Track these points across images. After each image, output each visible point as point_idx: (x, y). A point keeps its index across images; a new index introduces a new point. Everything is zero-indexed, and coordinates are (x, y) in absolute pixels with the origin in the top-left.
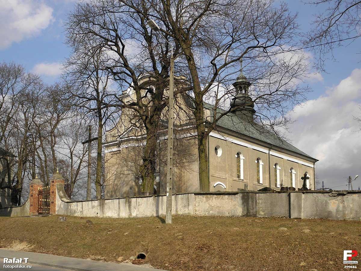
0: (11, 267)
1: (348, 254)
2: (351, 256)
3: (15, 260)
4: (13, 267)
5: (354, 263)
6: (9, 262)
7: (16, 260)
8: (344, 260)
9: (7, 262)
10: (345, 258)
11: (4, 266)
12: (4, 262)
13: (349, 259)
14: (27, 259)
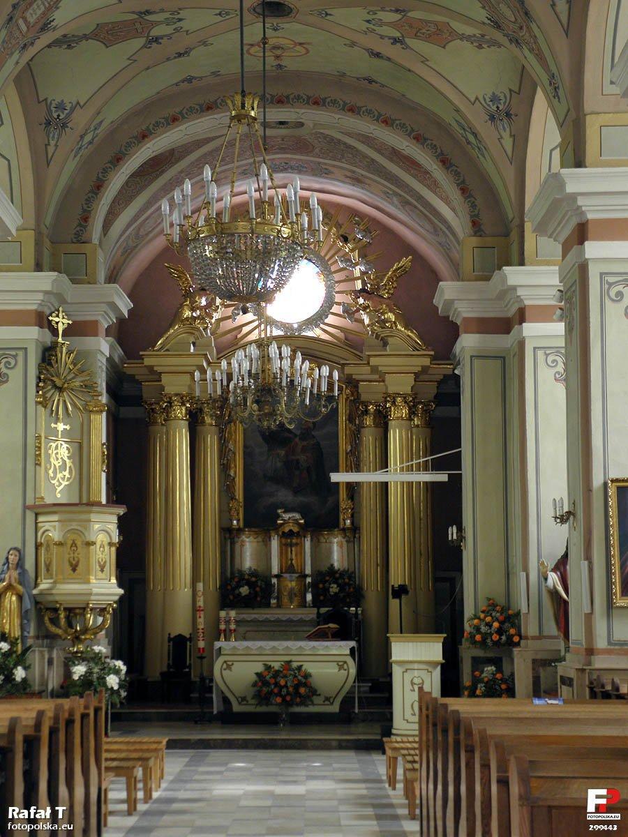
0: (24, 827)
1: (598, 797)
2: (605, 803)
3: (35, 811)
4: (31, 827)
5: (611, 819)
6: (21, 816)
7: (38, 811)
8: (588, 811)
9: (16, 817)
10: (591, 808)
11: (9, 825)
12: (10, 817)
13: (598, 808)
14: (63, 810)
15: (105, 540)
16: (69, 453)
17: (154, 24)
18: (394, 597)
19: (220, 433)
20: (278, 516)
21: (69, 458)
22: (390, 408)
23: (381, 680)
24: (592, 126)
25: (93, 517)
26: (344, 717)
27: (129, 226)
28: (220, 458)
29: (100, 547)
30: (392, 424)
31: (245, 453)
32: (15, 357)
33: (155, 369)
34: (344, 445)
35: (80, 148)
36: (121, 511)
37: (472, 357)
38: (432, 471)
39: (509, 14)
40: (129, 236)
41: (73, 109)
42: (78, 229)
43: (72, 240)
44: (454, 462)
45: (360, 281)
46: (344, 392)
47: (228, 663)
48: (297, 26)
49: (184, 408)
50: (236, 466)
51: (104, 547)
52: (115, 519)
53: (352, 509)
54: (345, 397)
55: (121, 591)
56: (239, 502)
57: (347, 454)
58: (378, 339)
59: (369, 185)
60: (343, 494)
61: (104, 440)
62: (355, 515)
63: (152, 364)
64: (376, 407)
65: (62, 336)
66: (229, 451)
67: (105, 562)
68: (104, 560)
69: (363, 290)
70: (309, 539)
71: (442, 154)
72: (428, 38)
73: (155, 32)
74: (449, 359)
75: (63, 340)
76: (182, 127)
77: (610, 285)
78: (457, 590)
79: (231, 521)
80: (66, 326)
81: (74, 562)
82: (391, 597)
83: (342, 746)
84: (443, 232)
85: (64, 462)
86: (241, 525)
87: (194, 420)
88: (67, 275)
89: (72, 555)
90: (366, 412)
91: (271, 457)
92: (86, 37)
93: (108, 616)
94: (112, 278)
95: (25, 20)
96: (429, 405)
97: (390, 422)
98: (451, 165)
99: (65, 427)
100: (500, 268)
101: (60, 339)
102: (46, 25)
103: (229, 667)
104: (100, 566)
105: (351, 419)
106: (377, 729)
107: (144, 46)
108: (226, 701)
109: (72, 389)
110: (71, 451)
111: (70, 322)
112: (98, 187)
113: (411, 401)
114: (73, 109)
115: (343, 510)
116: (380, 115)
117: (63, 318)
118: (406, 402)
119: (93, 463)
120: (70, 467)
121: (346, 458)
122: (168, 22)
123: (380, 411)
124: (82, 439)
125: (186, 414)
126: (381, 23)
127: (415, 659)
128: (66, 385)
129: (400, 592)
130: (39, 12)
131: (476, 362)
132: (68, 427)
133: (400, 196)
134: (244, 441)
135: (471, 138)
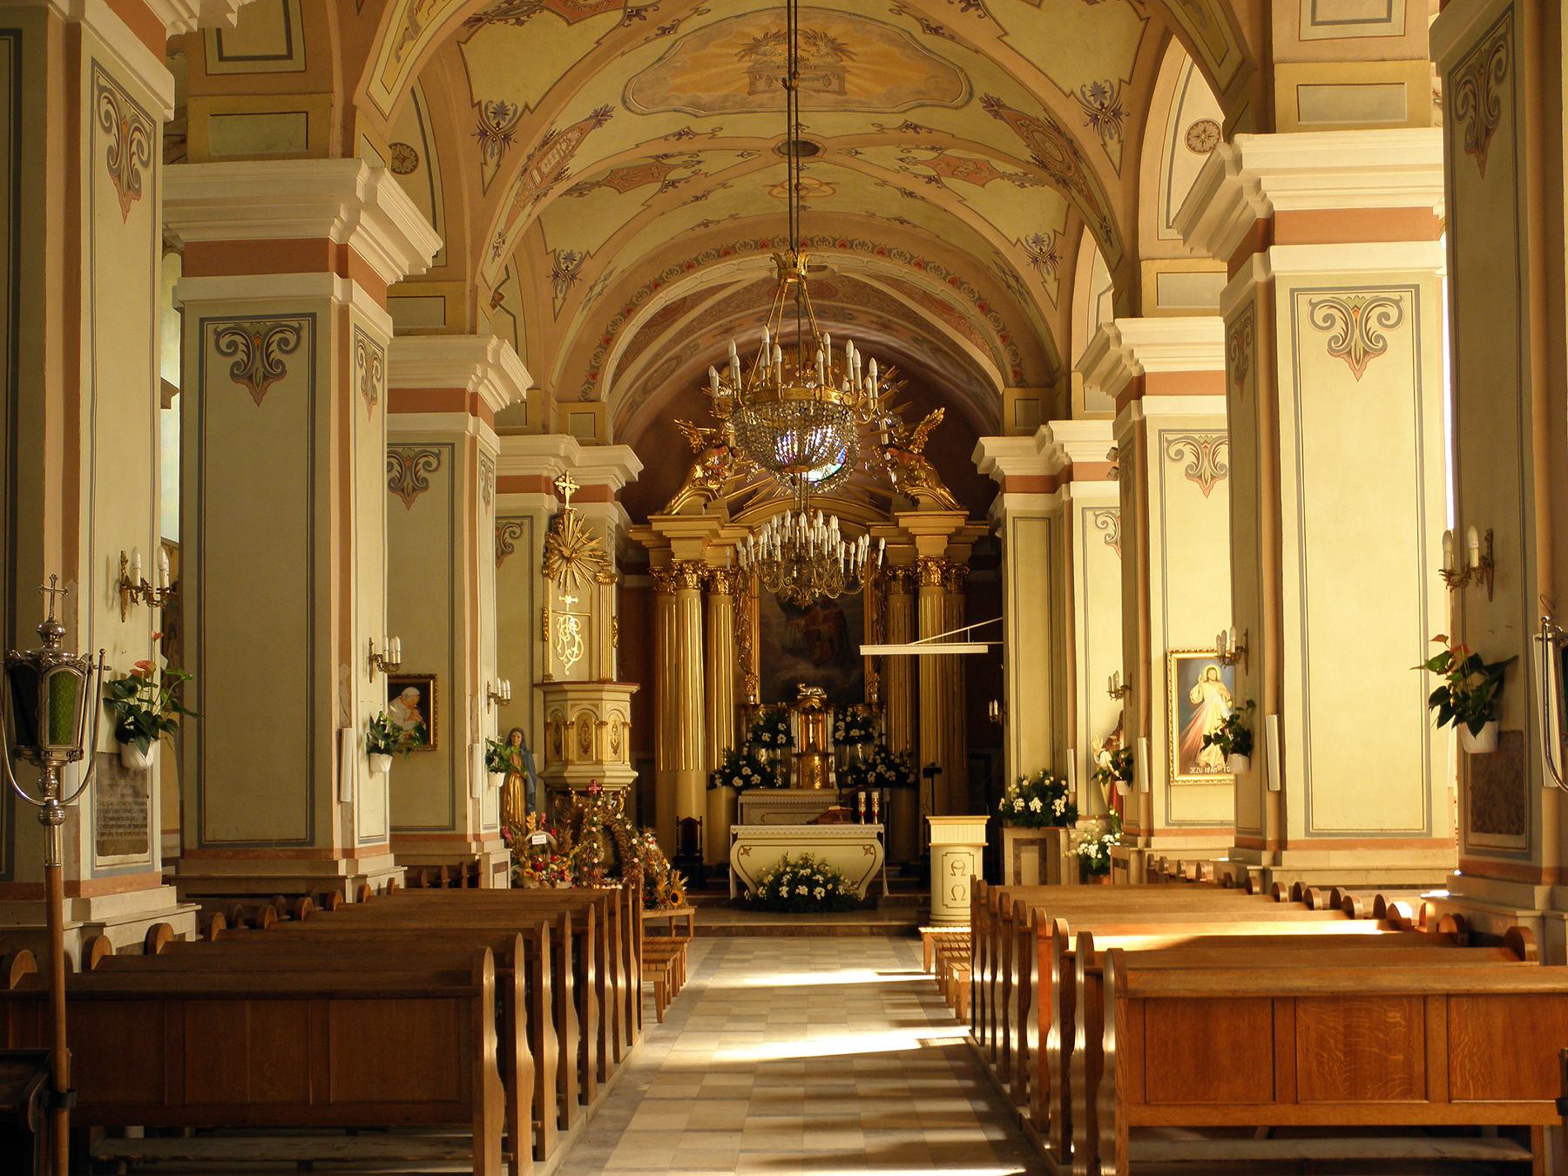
17: (673, 167)
20: (799, 691)
24: (1148, 271)
25: (605, 695)
26: (870, 904)
27: (637, 379)
28: (735, 630)
30: (923, 590)
31: (761, 624)
32: (520, 525)
34: (870, 614)
36: (635, 688)
39: (1056, 153)
41: (582, 260)
44: (995, 633)
48: (825, 166)
52: (627, 697)
60: (868, 667)
69: (890, 445)
71: (980, 298)
72: (967, 177)
73: (672, 176)
76: (698, 274)
77: (1170, 443)
83: (874, 933)
87: (707, 588)
90: (895, 577)
92: (598, 184)
94: (618, 440)
95: (539, 170)
100: (1045, 423)
102: (560, 174)
103: (746, 852)
106: (913, 914)
107: (661, 191)
108: (741, 886)
112: (608, 341)
114: (582, 260)
116: (912, 257)
119: (603, 638)
122: (686, 165)
126: (916, 162)
127: (958, 840)
129: (931, 772)
130: (553, 162)
131: (1020, 524)
135: (1012, 282)
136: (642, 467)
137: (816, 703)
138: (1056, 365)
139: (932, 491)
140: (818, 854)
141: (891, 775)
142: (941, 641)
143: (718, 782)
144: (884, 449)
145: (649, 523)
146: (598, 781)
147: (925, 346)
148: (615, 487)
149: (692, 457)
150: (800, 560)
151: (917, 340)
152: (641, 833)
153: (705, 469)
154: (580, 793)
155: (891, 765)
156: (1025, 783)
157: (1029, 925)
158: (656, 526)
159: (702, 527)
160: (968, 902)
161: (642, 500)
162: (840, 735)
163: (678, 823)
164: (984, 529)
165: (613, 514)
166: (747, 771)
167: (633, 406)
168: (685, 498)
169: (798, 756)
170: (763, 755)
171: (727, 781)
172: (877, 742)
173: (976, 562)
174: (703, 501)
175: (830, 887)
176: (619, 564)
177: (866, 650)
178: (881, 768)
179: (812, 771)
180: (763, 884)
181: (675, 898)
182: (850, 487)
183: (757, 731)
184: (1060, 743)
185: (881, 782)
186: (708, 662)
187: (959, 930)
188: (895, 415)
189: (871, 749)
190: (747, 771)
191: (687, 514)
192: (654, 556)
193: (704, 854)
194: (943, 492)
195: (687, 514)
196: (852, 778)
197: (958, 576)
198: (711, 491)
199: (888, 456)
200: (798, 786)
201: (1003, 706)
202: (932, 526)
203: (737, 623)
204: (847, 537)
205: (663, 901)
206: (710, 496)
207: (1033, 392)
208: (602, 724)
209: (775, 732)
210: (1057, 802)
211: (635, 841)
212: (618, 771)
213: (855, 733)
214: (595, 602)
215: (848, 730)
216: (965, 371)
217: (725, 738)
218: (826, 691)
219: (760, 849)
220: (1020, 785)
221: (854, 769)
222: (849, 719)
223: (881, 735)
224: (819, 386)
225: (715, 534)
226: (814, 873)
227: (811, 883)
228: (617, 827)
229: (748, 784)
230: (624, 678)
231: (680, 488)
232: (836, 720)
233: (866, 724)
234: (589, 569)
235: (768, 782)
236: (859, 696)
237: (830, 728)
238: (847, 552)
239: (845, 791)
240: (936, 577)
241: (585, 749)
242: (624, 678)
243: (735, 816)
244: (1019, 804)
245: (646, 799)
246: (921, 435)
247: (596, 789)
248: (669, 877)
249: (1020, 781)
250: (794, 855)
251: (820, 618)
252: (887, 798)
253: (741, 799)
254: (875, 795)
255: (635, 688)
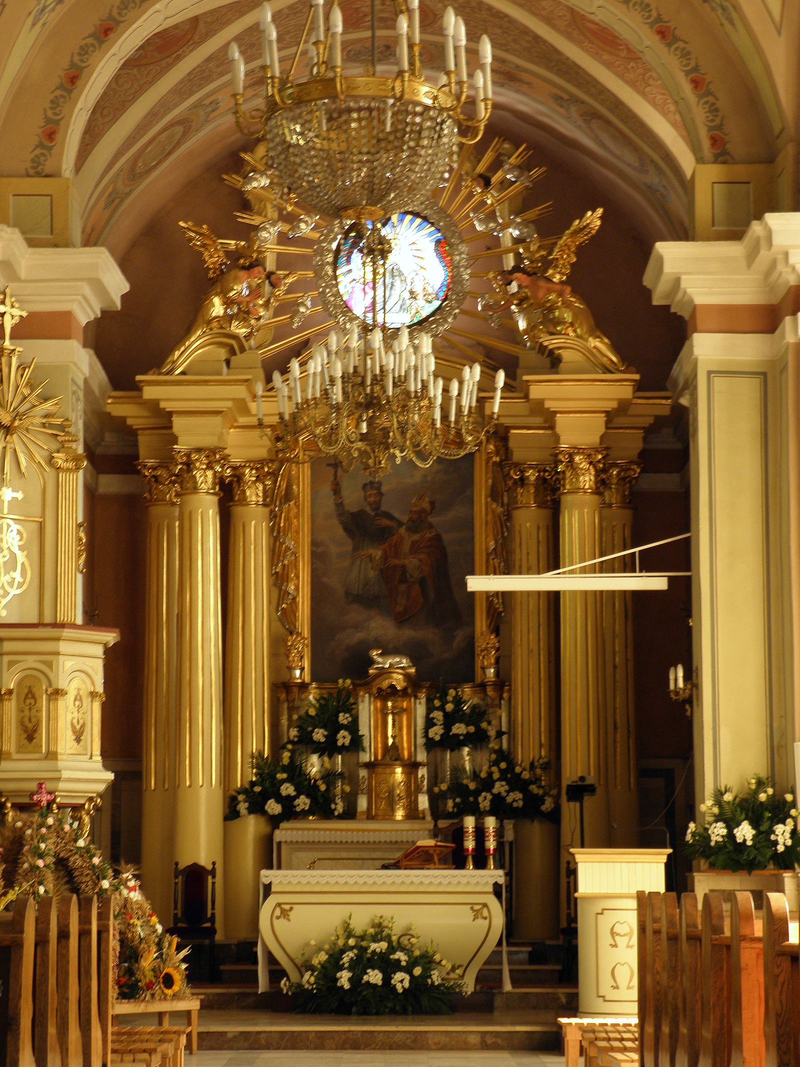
15: (83, 687)
16: (21, 540)
18: (569, 799)
19: (271, 520)
20: (372, 662)
21: (21, 548)
22: (564, 472)
23: (548, 942)
25: (63, 647)
26: (482, 1004)
28: (272, 562)
29: (75, 700)
30: (567, 500)
31: (314, 554)
33: (163, 405)
35: (43, 10)
36: (111, 637)
37: (710, 373)
38: (641, 571)
40: (117, 175)
42: (38, 151)
43: (26, 170)
44: (679, 558)
45: (511, 255)
46: (483, 448)
47: (284, 906)
49: (210, 473)
50: (298, 578)
51: (81, 700)
52: (99, 651)
53: (498, 650)
54: (484, 457)
55: (110, 776)
56: (303, 638)
57: (488, 555)
58: (543, 354)
59: (528, 84)
61: (80, 519)
62: (501, 660)
63: (158, 397)
64: (539, 471)
65: (11, 338)
66: (285, 552)
67: (83, 726)
68: (81, 722)
69: (516, 269)
70: (423, 701)
71: (659, 19)
74: (663, 388)
75: (12, 344)
78: (677, 791)
79: (290, 669)
80: (16, 320)
81: (30, 726)
82: (564, 797)
84: (656, 166)
85: (13, 556)
86: (307, 679)
87: (228, 494)
88: (23, 232)
89: (27, 712)
90: (522, 481)
91: (358, 562)
93: (87, 819)
94: (90, 240)
96: (629, 469)
97: (563, 498)
98: (676, 39)
99: (15, 495)
100: (759, 217)
101: (7, 343)
103: (285, 914)
104: (74, 732)
105: (494, 494)
108: (276, 972)
109: (27, 430)
110: (25, 536)
111: (25, 314)
112: (73, 79)
113: (599, 461)
115: (482, 651)
117: (13, 307)
118: (591, 463)
119: (62, 557)
120: (23, 564)
121: (487, 561)
123: (544, 480)
124: (43, 515)
125: (214, 484)
127: (617, 882)
128: (17, 423)
129: (578, 791)
132: (20, 495)
133: (583, 102)
134: (312, 535)
136: (125, 287)
137: (398, 680)
138: (777, 127)
139: (581, 342)
140: (401, 919)
141: (516, 798)
142: (593, 569)
143: (243, 807)
144: (507, 277)
145: (137, 388)
146: (49, 786)
147: (573, 109)
148: (84, 316)
149: (210, 282)
150: (372, 403)
151: (562, 100)
152: (117, 873)
153: (228, 303)
154: (20, 808)
155: (515, 782)
156: (728, 797)
157: (727, 933)
158: (149, 393)
159: (221, 395)
160: (634, 994)
161: (129, 345)
162: (436, 732)
163: (177, 873)
164: (661, 406)
165: (80, 362)
166: (288, 789)
167: (114, 200)
168: (195, 348)
169: (370, 766)
170: (314, 765)
171: (257, 808)
172: (493, 745)
173: (649, 459)
174: (223, 353)
175: (417, 971)
176: (90, 453)
177: (477, 583)
178: (500, 787)
179: (391, 792)
180: (312, 968)
181: (168, 981)
182: (455, 339)
183: (305, 725)
184: (783, 734)
185: (499, 808)
186: (229, 614)
187: (621, 1021)
188: (525, 223)
189: (484, 760)
190: (288, 789)
191: (197, 375)
192: (145, 442)
193: (219, 925)
194: (599, 344)
195: (197, 375)
196: (454, 801)
197: (622, 479)
198: (235, 337)
199: (514, 287)
200: (370, 816)
201: (691, 675)
202: (582, 399)
203: (276, 553)
204: (448, 370)
205: (150, 986)
206: (234, 348)
207: (741, 171)
208: (58, 693)
209: (334, 728)
210: (779, 828)
211: (105, 884)
212: (81, 770)
213: (459, 729)
214: (49, 501)
215: (447, 726)
216: (636, 149)
217: (255, 739)
218: (415, 662)
219: (309, 909)
220: (719, 802)
221: (457, 788)
222: (449, 707)
223: (500, 734)
224: (400, 73)
225: (242, 407)
226: (392, 949)
227: (388, 966)
228: (76, 861)
229: (289, 813)
230: (94, 617)
231: (188, 331)
232: (430, 709)
233: (477, 716)
234: (40, 446)
235: (322, 808)
236: (463, 668)
237: (420, 722)
238: (446, 390)
239: (443, 824)
240: (587, 480)
241: (30, 733)
242: (94, 617)
243: (269, 855)
244: (718, 831)
245: (127, 820)
246: (565, 252)
247: (45, 799)
248: (159, 945)
249: (719, 795)
250: (361, 920)
251: (406, 547)
252: (509, 836)
253: (279, 835)
254: (491, 823)
255: (111, 637)
